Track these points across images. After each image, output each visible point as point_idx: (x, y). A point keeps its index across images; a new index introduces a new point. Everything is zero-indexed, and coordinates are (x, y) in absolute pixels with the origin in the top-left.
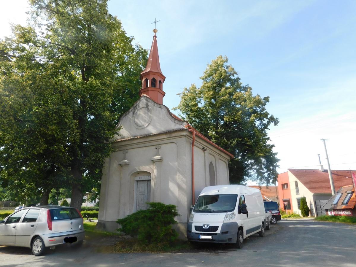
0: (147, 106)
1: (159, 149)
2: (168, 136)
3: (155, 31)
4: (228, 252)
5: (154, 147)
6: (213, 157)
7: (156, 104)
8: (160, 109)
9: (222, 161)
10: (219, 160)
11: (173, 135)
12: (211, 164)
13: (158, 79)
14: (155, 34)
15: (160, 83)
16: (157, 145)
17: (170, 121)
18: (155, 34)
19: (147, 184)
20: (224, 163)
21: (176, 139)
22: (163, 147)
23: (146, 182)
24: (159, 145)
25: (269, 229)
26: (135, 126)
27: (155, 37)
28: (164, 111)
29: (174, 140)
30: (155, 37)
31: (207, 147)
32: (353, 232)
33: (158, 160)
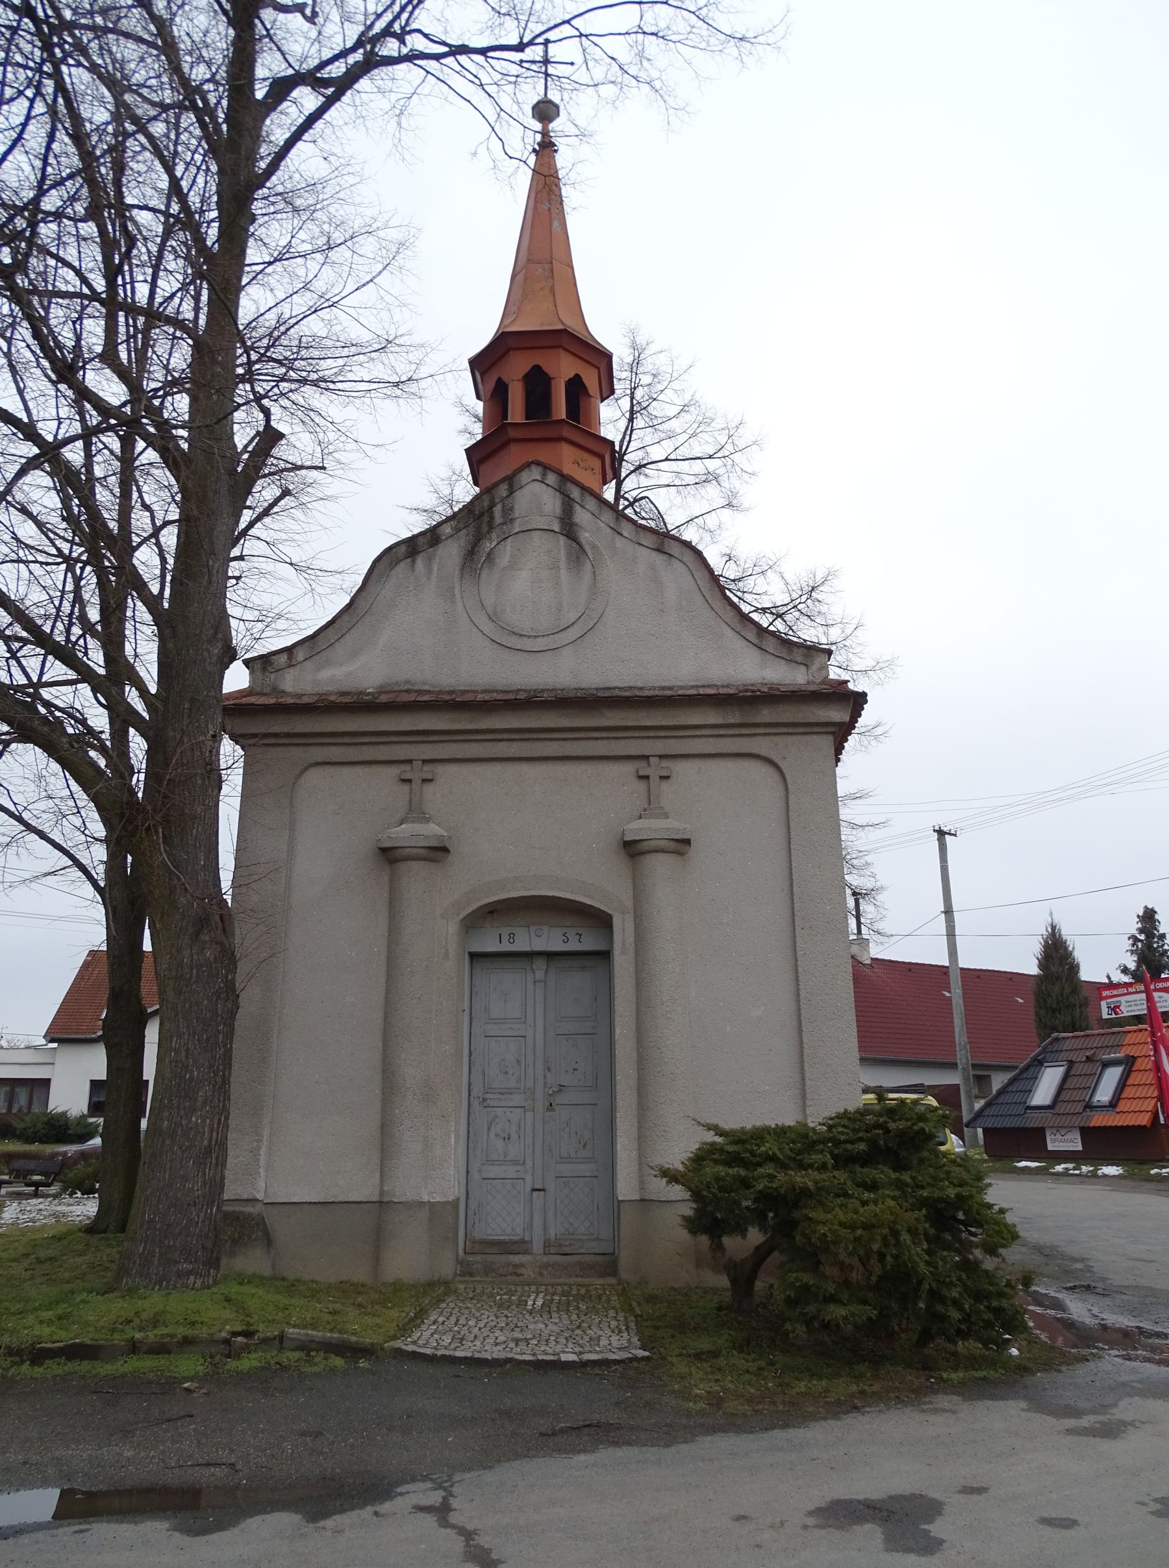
2: (734, 717)
5: (628, 768)
11: (766, 714)
17: (729, 633)
18: (545, 133)
30: (546, 147)
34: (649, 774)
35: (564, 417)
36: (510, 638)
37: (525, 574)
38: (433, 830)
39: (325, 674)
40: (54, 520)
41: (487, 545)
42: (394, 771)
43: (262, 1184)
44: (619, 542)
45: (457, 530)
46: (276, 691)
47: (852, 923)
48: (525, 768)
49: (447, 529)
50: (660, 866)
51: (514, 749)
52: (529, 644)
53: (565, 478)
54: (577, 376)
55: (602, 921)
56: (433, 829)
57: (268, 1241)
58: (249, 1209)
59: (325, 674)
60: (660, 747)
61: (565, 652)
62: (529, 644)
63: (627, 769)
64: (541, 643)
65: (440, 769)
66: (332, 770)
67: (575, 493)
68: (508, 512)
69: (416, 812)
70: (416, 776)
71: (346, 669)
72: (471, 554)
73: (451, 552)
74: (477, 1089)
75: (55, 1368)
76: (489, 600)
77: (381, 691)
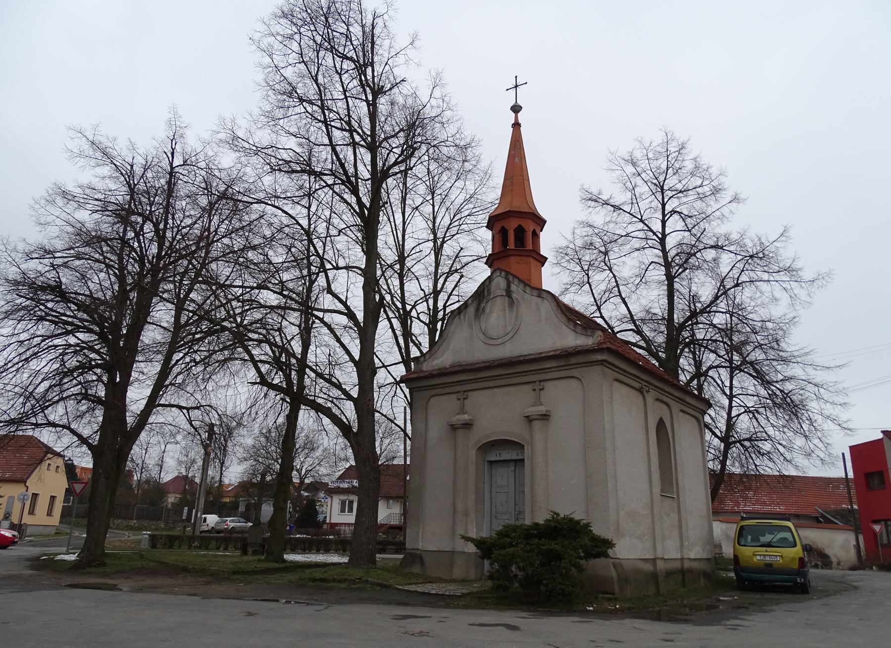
0: (509, 293)
1: (542, 392)
2: (562, 363)
3: (516, 109)
4: (774, 607)
5: (529, 387)
6: (665, 407)
7: (528, 290)
8: (539, 300)
9: (687, 416)
10: (681, 414)
11: (573, 360)
12: (661, 424)
13: (530, 226)
14: (516, 118)
15: (536, 236)
16: (534, 382)
17: (564, 327)
18: (516, 118)
19: (513, 468)
20: (693, 420)
21: (702, 476)
22: (549, 385)
23: (512, 464)
24: (540, 381)
25: (850, 447)
26: (481, 335)
27: (516, 125)
28: (547, 307)
29: (575, 372)
30: (516, 125)
31: (651, 384)
32: (472, 516)
33: (540, 417)
34: (538, 387)
35: (513, 247)
36: (490, 340)
37: (494, 315)
38: (542, 409)
39: (435, 363)
40: (37, 433)
41: (483, 305)
42: (455, 396)
43: (420, 544)
44: (526, 296)
45: (473, 301)
46: (422, 371)
47: (408, 448)
48: (496, 390)
49: (470, 301)
50: (537, 425)
51: (491, 384)
52: (495, 342)
53: (508, 273)
54: (520, 226)
55: (520, 446)
56: (466, 417)
57: (422, 563)
58: (417, 552)
59: (435, 363)
60: (465, 388)
61: (508, 343)
62: (495, 342)
63: (529, 387)
64: (500, 341)
65: (470, 393)
66: (438, 397)
67: (511, 278)
68: (489, 290)
69: (462, 411)
70: (462, 398)
71: (441, 359)
72: (477, 309)
73: (471, 310)
74: (494, 512)
75: (317, 583)
76: (483, 327)
77: (452, 366)
